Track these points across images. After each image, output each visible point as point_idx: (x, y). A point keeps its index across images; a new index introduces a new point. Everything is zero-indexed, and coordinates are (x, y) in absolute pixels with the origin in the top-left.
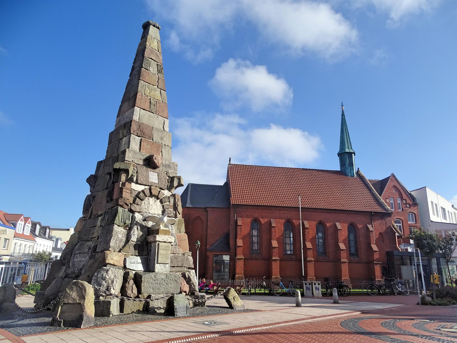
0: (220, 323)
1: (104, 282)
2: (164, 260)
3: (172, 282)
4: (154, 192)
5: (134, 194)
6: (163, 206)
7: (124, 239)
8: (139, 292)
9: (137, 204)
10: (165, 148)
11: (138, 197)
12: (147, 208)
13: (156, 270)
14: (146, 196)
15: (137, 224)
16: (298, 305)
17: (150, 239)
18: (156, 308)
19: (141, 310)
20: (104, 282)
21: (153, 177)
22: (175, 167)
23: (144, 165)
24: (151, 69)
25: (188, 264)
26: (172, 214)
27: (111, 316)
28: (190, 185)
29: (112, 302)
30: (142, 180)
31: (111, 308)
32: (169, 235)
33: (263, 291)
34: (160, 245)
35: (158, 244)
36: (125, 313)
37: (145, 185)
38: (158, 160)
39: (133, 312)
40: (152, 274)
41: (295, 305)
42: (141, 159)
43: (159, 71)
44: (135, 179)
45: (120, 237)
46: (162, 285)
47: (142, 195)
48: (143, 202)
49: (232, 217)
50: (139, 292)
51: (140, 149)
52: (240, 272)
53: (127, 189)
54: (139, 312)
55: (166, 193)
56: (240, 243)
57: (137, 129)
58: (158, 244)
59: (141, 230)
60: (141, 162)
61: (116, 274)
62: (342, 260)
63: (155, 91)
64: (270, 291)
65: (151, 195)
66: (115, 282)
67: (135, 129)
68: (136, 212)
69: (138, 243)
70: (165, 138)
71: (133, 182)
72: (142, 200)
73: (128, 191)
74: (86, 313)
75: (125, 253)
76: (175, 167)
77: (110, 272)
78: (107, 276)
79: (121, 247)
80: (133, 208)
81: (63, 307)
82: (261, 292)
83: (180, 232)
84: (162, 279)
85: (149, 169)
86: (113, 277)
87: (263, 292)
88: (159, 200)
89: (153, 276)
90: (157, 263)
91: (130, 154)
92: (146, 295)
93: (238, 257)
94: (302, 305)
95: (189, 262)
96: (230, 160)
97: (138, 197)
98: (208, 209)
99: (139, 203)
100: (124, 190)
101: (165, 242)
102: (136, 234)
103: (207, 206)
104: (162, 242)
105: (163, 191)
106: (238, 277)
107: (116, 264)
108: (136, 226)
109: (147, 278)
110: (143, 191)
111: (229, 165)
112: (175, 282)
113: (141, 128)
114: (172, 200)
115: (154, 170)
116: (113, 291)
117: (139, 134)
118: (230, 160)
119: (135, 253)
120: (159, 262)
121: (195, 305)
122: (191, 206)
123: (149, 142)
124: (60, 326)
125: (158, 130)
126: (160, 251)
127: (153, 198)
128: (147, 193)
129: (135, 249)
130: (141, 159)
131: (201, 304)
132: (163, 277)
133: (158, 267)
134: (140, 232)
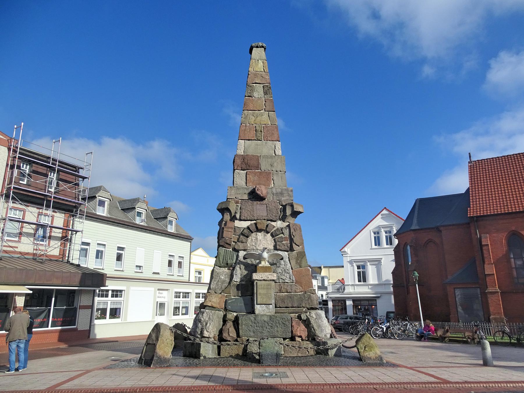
0: (197, 378)
1: (200, 325)
2: (264, 300)
3: (278, 325)
4: (259, 227)
5: (238, 232)
6: (275, 240)
7: (228, 280)
8: (238, 335)
9: (242, 242)
10: (277, 174)
11: (246, 233)
12: (254, 244)
13: (257, 312)
14: (252, 232)
15: (241, 263)
16: (486, 364)
17: (255, 276)
18: (255, 353)
19: (241, 354)
20: (200, 325)
21: (260, 210)
22: (290, 193)
23: (249, 199)
24: (256, 94)
25: (309, 304)
26: (286, 247)
27: (202, 358)
28: (418, 201)
29: (202, 345)
30: (246, 215)
31: (201, 350)
32: (270, 272)
33: (506, 339)
34: (258, 284)
35: (257, 283)
36: (221, 356)
37: (251, 220)
38: (262, 191)
39: (231, 356)
40: (252, 317)
41: (481, 362)
42: (245, 194)
43: (265, 93)
44: (238, 216)
45: (223, 278)
46: (265, 329)
47: (246, 231)
48: (249, 239)
49: (473, 235)
50: (238, 335)
51: (246, 184)
52: (495, 312)
53: (229, 228)
54: (237, 357)
55: (279, 224)
56: (490, 269)
57: (242, 163)
58: (257, 283)
59: (245, 269)
60: (246, 197)
61: (211, 317)
62: (490, 290)
63: (262, 115)
64: (518, 340)
65: (258, 230)
66: (208, 324)
67: (240, 163)
68: (241, 250)
69: (243, 283)
70: (275, 164)
71: (237, 219)
72: (247, 237)
73: (230, 230)
74: (157, 354)
75: (226, 295)
76: (290, 193)
77: (205, 315)
78: (202, 319)
79: (223, 288)
80: (236, 247)
81: (148, 347)
82: (503, 341)
83: (301, 267)
84: (265, 321)
85: (255, 203)
86: (207, 319)
87: (507, 341)
88: (269, 234)
89: (252, 318)
90: (257, 304)
91: (233, 191)
92: (245, 338)
93: (490, 290)
94: (495, 363)
95: (311, 301)
96: (470, 157)
97: (246, 233)
98: (441, 228)
99: (244, 241)
100: (225, 229)
101: (264, 280)
102: (239, 274)
103: (438, 224)
104: (260, 280)
105: (273, 224)
106: (495, 319)
107: (214, 305)
108: (239, 266)
109: (245, 321)
110: (248, 228)
111: (469, 163)
112: (283, 325)
113: (246, 160)
114: (286, 232)
115: (262, 202)
116: (206, 334)
117: (244, 166)
118: (470, 157)
119: (238, 293)
120: (258, 303)
121: (318, 352)
122: (417, 228)
123: (255, 174)
124: (142, 364)
125: (266, 157)
126: (260, 291)
127: (263, 232)
128: (253, 228)
129: (238, 290)
130: (245, 194)
131: (324, 352)
132: (266, 319)
133: (258, 309)
134: (244, 271)
